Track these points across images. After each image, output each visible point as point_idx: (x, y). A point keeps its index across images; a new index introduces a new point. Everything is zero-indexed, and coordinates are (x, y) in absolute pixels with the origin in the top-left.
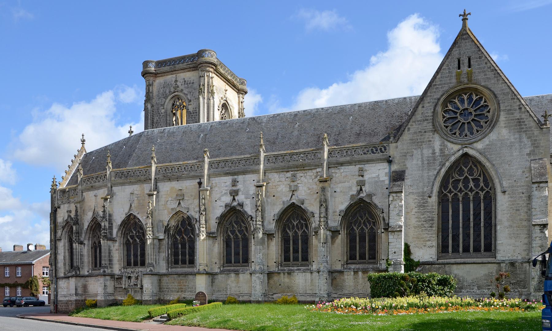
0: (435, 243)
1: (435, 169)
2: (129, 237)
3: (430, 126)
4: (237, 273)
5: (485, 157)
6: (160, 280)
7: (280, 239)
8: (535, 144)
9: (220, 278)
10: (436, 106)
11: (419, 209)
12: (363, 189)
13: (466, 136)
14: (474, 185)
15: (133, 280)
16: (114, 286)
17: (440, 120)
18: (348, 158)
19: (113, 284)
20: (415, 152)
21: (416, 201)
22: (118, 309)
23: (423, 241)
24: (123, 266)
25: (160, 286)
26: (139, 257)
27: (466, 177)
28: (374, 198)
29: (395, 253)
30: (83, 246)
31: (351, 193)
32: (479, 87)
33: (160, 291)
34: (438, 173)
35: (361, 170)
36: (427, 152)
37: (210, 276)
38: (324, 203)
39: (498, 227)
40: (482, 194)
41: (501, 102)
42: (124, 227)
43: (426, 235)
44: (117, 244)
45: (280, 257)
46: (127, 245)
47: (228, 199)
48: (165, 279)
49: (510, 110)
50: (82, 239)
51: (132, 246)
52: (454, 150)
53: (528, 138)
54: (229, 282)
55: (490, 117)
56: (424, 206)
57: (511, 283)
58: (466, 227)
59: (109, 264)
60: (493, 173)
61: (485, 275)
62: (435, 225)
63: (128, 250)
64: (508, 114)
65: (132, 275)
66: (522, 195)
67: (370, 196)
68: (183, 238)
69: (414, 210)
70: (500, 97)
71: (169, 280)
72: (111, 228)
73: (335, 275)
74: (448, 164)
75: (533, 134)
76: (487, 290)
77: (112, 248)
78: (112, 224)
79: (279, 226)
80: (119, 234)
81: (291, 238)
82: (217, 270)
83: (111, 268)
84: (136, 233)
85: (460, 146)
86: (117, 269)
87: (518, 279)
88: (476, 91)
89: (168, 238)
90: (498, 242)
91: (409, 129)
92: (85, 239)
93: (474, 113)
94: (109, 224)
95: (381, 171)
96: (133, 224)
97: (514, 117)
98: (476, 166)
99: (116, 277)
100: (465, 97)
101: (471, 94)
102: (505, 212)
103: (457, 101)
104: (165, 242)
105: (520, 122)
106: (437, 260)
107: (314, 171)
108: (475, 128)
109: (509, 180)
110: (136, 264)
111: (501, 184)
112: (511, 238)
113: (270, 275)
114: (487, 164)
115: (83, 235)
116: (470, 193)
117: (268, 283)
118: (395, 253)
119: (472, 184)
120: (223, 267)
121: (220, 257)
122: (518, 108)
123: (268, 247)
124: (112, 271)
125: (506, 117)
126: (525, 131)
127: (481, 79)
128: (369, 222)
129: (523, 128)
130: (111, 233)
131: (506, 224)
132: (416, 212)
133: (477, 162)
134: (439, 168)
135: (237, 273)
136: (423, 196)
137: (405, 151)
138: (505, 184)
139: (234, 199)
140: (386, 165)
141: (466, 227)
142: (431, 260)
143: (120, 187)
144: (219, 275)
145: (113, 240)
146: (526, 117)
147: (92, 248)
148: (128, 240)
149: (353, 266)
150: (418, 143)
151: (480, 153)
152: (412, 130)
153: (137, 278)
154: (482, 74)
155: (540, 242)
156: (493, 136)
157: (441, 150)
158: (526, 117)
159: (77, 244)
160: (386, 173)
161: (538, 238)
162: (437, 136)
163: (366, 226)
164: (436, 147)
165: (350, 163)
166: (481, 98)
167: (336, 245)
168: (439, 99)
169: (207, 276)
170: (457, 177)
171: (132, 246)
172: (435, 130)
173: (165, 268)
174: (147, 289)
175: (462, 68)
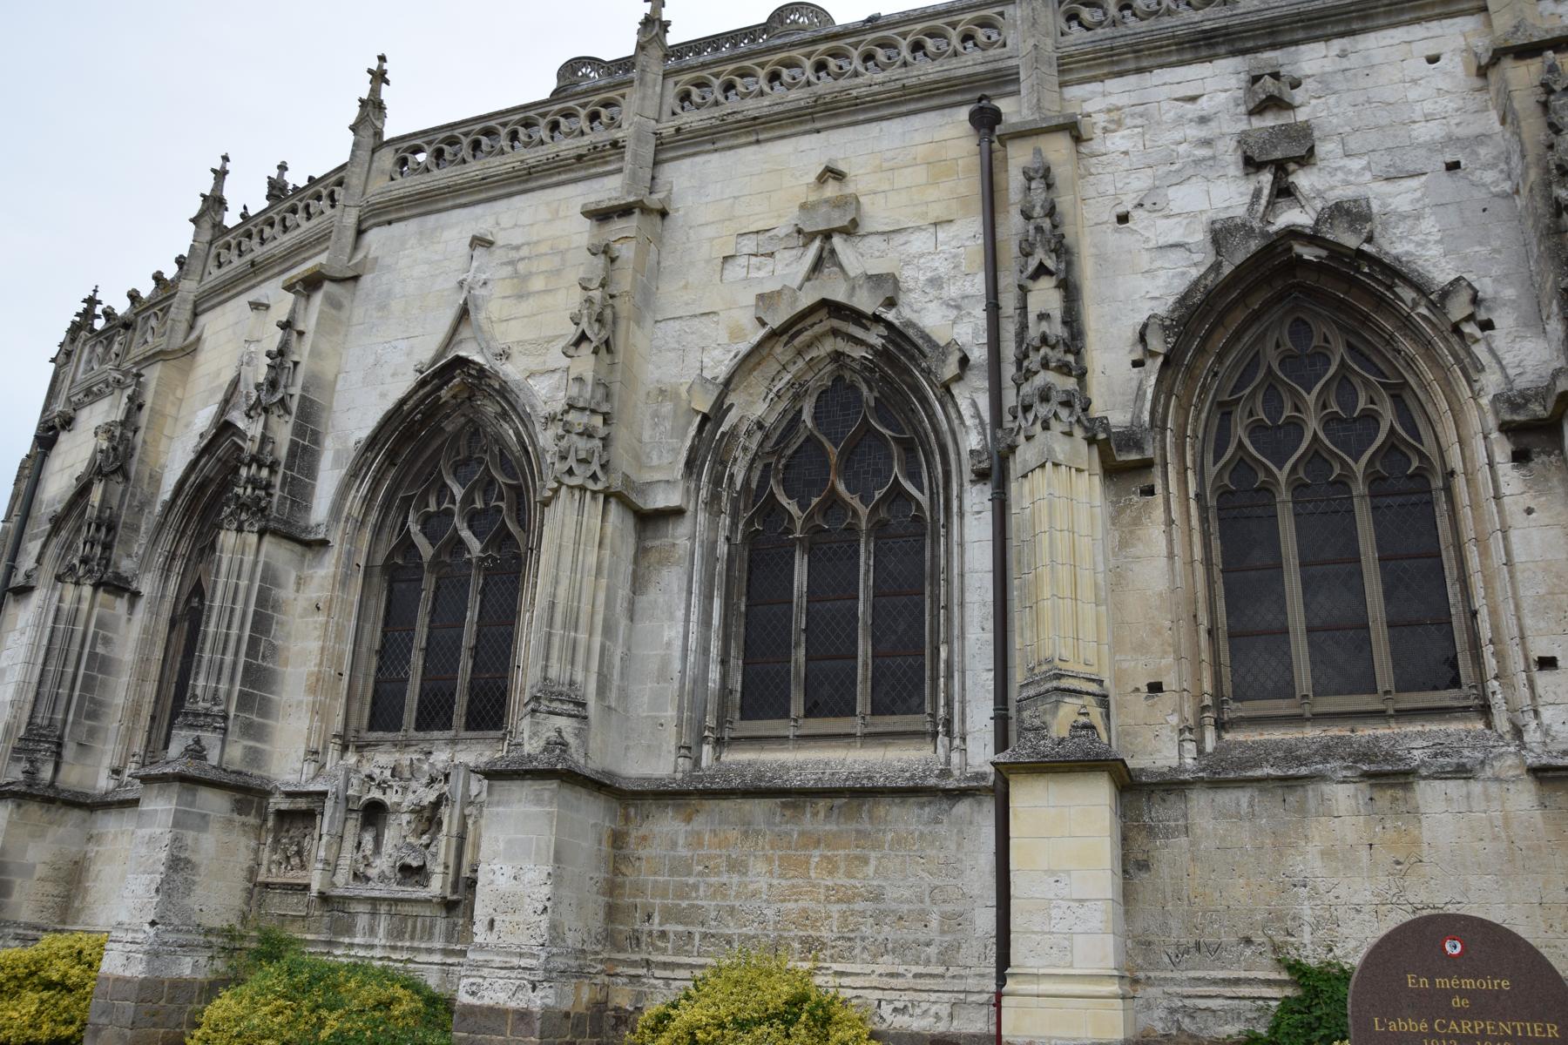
2: (414, 528)
4: (1389, 777)
6: (618, 839)
15: (396, 832)
16: (252, 872)
19: (244, 859)
22: (1101, 258)
24: (337, 725)
25: (612, 888)
26: (466, 664)
30: (121, 605)
33: (610, 938)
42: (391, 458)
44: (326, 568)
46: (394, 575)
47: (1231, 194)
48: (666, 831)
50: (126, 566)
51: (428, 583)
54: (1308, 860)
59: (245, 701)
63: (396, 621)
65: (390, 798)
68: (833, 503)
71: (696, 841)
72: (304, 454)
77: (287, 592)
78: (316, 438)
83: (249, 730)
84: (468, 499)
86: (290, 754)
92: (144, 564)
94: (299, 430)
96: (456, 436)
99: (278, 803)
104: (680, 536)
110: (434, 716)
115: (139, 545)
120: (1221, 726)
124: (254, 756)
130: (300, 493)
135: (1389, 777)
143: (412, 226)
147: (173, 623)
148: (406, 545)
153: (429, 818)
159: (87, 591)
171: (428, 583)
174: (510, 904)
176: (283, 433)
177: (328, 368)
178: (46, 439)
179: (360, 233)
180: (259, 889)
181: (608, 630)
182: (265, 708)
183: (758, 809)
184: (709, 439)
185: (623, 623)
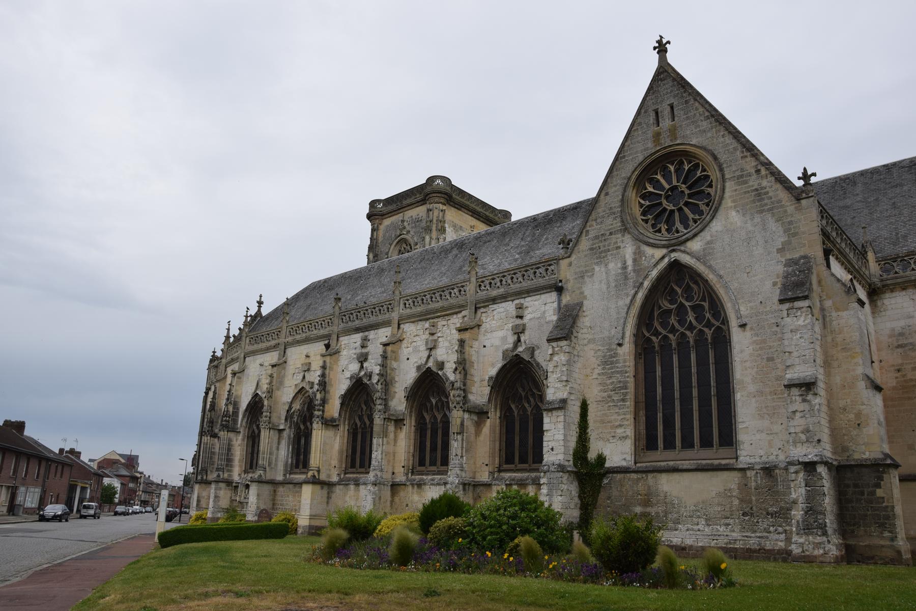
0: (630, 432)
1: (627, 295)
3: (617, 224)
5: (704, 263)
6: (275, 491)
7: (413, 428)
8: (790, 229)
9: (338, 489)
10: (625, 191)
11: (603, 369)
12: (522, 339)
13: (678, 232)
14: (696, 319)
17: (637, 211)
18: (502, 291)
19: (229, 495)
20: (597, 268)
21: (600, 353)
23: (612, 427)
27: (682, 305)
28: (537, 353)
29: (552, 449)
30: (216, 440)
31: (506, 347)
32: (688, 148)
34: (631, 301)
35: (520, 307)
36: (614, 266)
37: (326, 487)
38: (463, 365)
39: (738, 396)
40: (709, 333)
41: (725, 166)
43: (615, 417)
44: (240, 437)
45: (411, 459)
47: (354, 367)
48: (281, 490)
49: (742, 176)
50: (216, 431)
52: (656, 258)
53: (777, 221)
54: (347, 498)
55: (713, 194)
56: (612, 363)
57: (768, 514)
58: (686, 400)
59: (227, 465)
60: (721, 292)
61: (719, 494)
62: (631, 396)
64: (739, 184)
66: (775, 329)
67: (532, 350)
69: (597, 371)
70: (723, 158)
72: (236, 413)
73: (479, 490)
74: (647, 284)
75: (786, 211)
76: (722, 529)
77: (234, 442)
78: (238, 409)
79: (412, 407)
80: (244, 424)
81: (429, 426)
82: (335, 479)
83: (229, 471)
85: (664, 251)
87: (782, 504)
88: (685, 153)
89: (290, 427)
90: (740, 426)
91: (588, 231)
93: (687, 192)
94: (234, 408)
95: (547, 307)
97: (749, 187)
98: (696, 283)
100: (672, 168)
101: (682, 163)
102: (748, 364)
103: (659, 177)
104: (285, 434)
105: (759, 195)
106: (635, 463)
107: (460, 315)
108: (691, 216)
109: (750, 302)
111: (738, 311)
112: (762, 417)
113: (395, 487)
114: (711, 277)
116: (688, 333)
117: (392, 501)
118: (552, 449)
119: (691, 317)
120: (345, 474)
121: (341, 457)
122: (753, 171)
123: (395, 440)
124: (230, 476)
125: (736, 190)
126: (771, 210)
127: (695, 136)
128: (533, 395)
129: (766, 204)
130: (235, 421)
131: (752, 388)
132: (599, 374)
133: (696, 277)
134: (633, 292)
136: (610, 344)
137: (582, 269)
138: (743, 310)
139: (362, 367)
140: (553, 296)
141: (686, 400)
142: (624, 464)
144: (338, 487)
145: (235, 431)
146: (769, 184)
149: (507, 475)
150: (599, 254)
151: (698, 259)
152: (592, 234)
154: (693, 127)
155: (802, 422)
156: (717, 226)
157: (635, 260)
158: (769, 184)
160: (554, 310)
161: (798, 414)
162: (628, 238)
163: (529, 402)
164: (627, 256)
165: (504, 298)
166: (696, 166)
167: (482, 438)
168: (629, 179)
169: (318, 487)
170: (666, 305)
172: (625, 230)
173: (282, 473)
175: (661, 124)
176: (231, 409)
177: (239, 393)
178: (207, 393)
179: (245, 358)
180: (232, 501)
181: (271, 454)
182: (231, 466)
183: (291, 486)
184: (289, 416)
185: (275, 452)
